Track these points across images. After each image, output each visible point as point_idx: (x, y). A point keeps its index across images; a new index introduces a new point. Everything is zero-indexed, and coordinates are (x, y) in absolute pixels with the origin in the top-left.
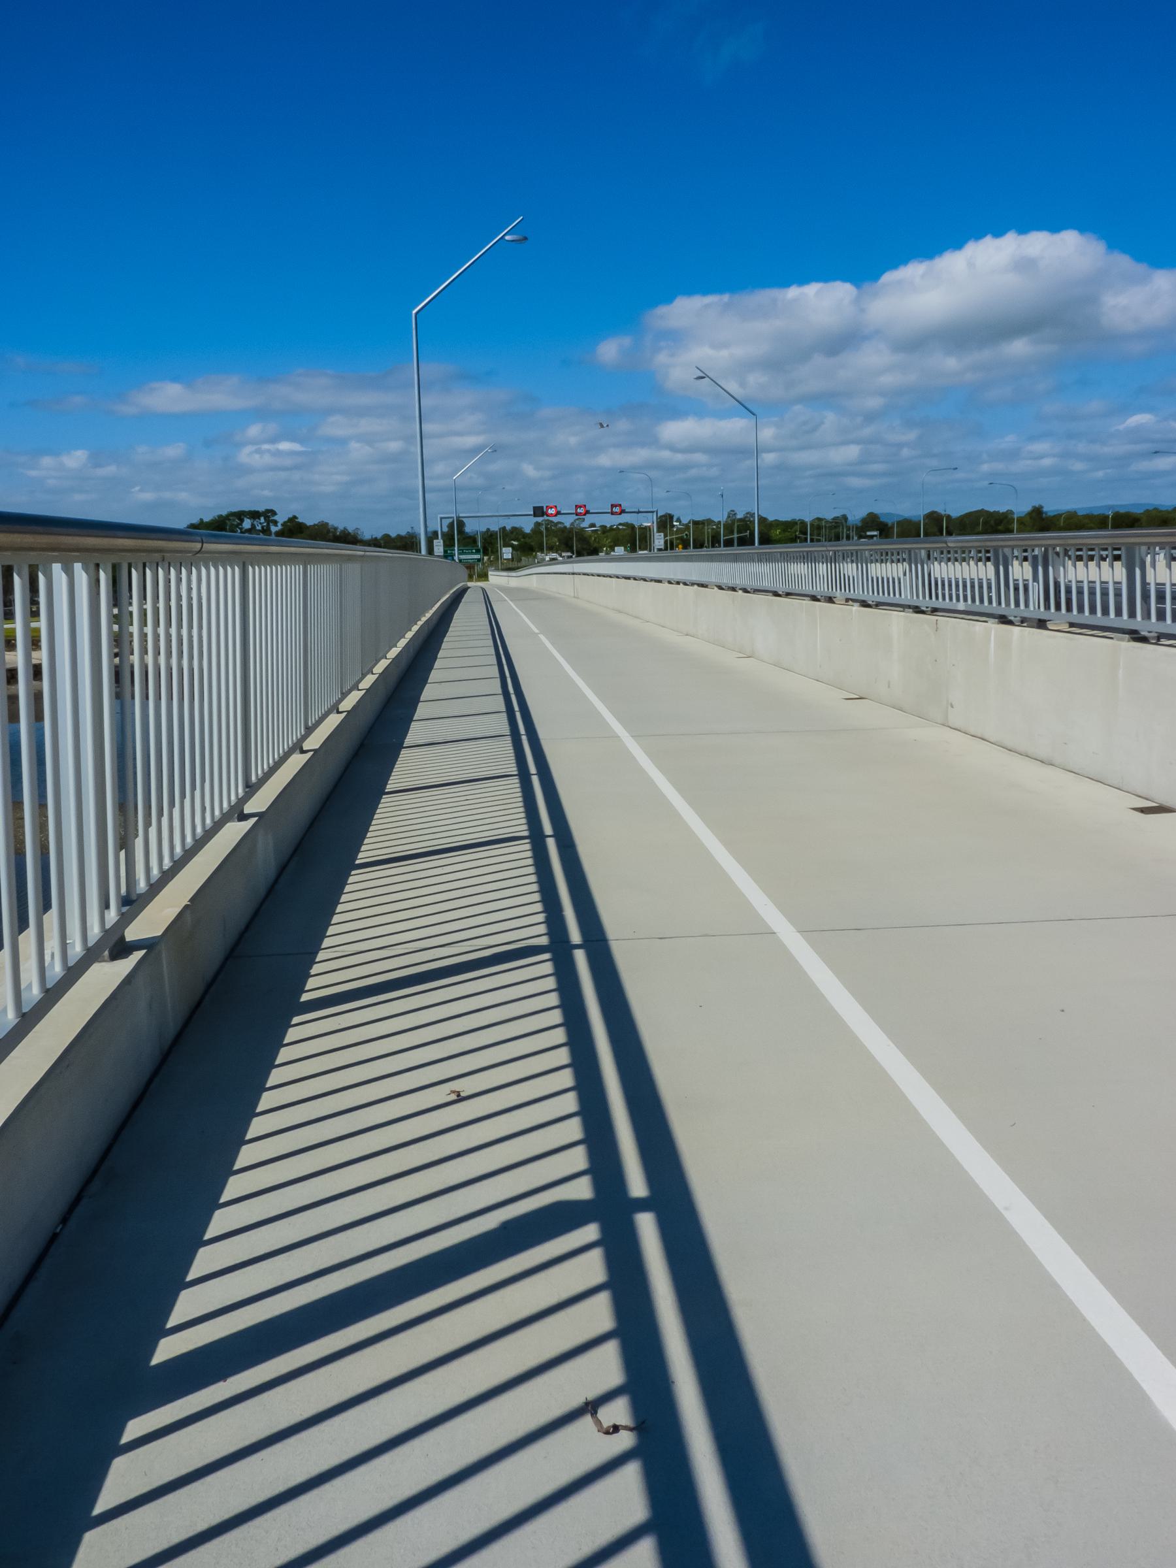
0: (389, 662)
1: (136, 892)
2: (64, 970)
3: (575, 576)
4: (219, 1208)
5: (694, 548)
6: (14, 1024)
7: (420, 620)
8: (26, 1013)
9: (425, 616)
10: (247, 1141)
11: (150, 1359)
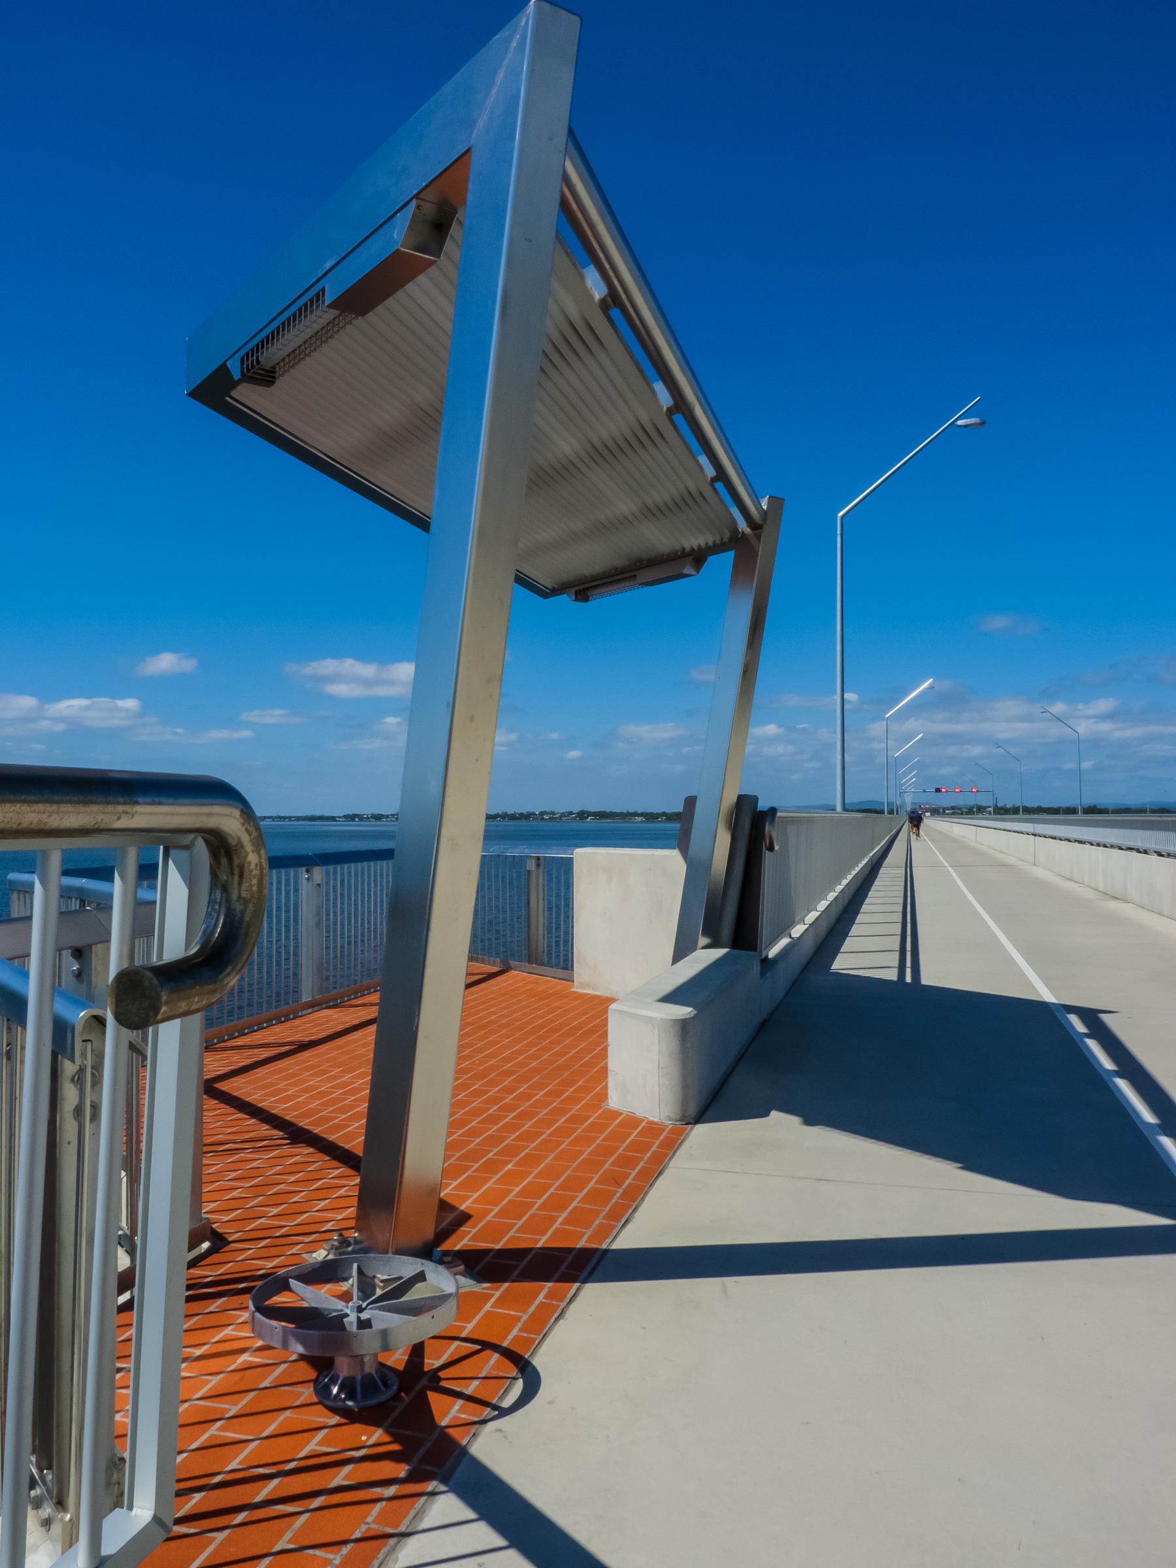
0: (818, 914)
3: (1037, 838)
5: (1023, 814)
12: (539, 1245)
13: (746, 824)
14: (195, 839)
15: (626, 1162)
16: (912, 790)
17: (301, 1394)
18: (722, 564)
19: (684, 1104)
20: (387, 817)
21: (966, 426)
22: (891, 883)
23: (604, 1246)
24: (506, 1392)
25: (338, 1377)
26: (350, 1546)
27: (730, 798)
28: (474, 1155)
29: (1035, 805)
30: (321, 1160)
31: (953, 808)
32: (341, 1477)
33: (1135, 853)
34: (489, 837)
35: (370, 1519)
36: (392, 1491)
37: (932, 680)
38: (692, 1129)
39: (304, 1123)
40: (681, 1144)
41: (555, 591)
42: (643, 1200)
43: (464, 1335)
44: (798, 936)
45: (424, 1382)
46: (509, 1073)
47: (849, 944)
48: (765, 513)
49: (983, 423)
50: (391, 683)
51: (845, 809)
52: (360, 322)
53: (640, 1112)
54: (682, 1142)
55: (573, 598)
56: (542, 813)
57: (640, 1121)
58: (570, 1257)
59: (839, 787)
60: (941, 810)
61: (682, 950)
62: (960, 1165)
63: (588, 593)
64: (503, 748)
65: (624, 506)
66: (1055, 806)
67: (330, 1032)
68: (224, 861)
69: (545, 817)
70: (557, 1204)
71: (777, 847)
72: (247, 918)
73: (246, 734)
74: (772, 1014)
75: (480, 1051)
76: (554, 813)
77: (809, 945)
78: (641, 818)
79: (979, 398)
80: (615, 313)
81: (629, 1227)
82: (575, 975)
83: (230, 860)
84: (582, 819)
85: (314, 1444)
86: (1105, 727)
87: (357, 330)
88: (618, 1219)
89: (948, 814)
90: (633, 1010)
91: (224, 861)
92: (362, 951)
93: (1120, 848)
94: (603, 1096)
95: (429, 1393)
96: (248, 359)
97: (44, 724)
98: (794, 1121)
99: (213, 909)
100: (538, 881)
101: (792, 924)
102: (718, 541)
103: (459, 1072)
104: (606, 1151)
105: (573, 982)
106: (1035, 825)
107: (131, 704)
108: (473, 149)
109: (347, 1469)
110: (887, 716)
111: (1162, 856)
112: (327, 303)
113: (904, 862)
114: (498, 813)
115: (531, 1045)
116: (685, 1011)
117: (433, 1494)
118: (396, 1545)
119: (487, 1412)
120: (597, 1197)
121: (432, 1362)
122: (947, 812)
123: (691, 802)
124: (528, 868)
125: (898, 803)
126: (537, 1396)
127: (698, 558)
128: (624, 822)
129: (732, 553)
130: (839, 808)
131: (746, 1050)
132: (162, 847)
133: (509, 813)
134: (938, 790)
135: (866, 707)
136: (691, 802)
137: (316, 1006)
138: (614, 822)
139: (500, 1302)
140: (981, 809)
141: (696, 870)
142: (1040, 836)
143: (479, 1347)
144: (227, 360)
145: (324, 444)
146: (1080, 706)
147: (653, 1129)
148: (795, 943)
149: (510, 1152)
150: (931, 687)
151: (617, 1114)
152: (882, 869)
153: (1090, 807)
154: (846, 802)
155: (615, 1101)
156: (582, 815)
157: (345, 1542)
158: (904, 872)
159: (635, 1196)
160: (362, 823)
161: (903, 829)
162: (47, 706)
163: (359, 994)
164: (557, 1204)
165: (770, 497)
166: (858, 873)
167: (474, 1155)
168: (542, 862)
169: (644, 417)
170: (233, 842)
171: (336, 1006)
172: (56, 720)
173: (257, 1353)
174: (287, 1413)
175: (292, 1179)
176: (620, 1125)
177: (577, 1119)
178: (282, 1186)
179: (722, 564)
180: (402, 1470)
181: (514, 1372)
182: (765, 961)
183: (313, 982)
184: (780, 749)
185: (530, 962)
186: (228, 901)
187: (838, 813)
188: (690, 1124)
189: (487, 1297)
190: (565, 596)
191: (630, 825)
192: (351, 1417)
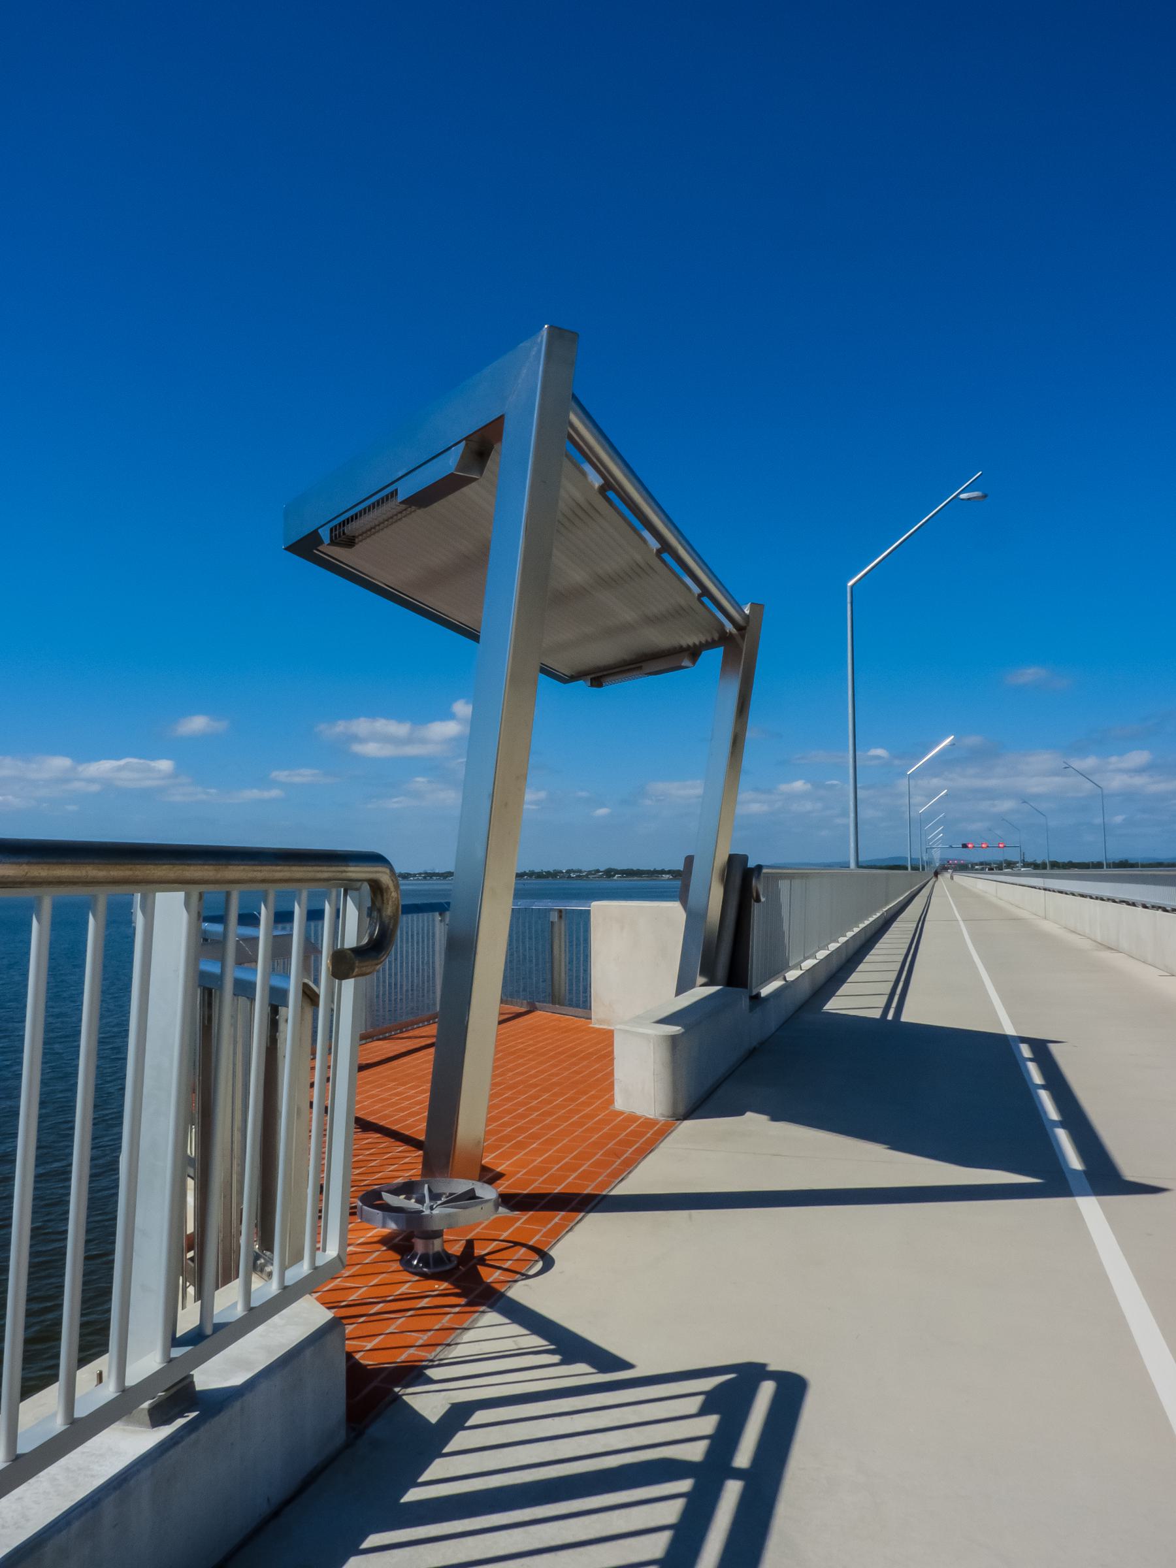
0: (816, 961)
1: (212, 1321)
2: (244, 1311)
3: (1047, 892)
4: (440, 1457)
5: (1107, 868)
6: (275, 1294)
7: (871, 917)
8: (255, 1307)
9: (876, 915)
10: (444, 1454)
11: (360, 1545)
12: (556, 1191)
13: (737, 881)
14: (361, 885)
15: (627, 1143)
16: (940, 846)
17: (391, 1266)
18: (713, 657)
19: (675, 1104)
20: (414, 875)
21: (969, 499)
22: (899, 936)
23: (604, 1193)
24: (530, 1268)
25: (417, 1254)
26: (432, 1332)
27: (722, 859)
28: (507, 1138)
29: (1066, 860)
30: (387, 1142)
31: (981, 864)
32: (424, 1303)
33: (1125, 906)
34: (518, 894)
35: (444, 1321)
36: (457, 1309)
37: (952, 737)
38: (680, 1124)
39: (371, 1119)
40: (670, 1134)
41: (573, 678)
42: (636, 1167)
43: (501, 1238)
44: (792, 979)
45: (475, 1261)
46: (535, 1085)
47: (845, 989)
48: (748, 616)
49: (985, 496)
50: (423, 741)
51: (858, 866)
52: (420, 512)
53: (639, 1112)
54: (672, 1132)
55: (589, 684)
56: (569, 872)
57: (637, 1118)
58: (578, 1199)
59: (852, 845)
60: (970, 866)
61: (683, 986)
62: (888, 1146)
63: (602, 680)
64: (534, 807)
65: (628, 615)
66: (1086, 861)
67: (383, 1057)
68: (379, 897)
69: (572, 875)
70: (570, 1168)
71: (763, 899)
72: (391, 927)
73: (275, 793)
74: (762, 1044)
75: (511, 1070)
76: (580, 871)
77: (806, 989)
78: (668, 876)
79: (980, 473)
80: (611, 494)
81: (623, 1183)
82: (593, 1013)
83: (382, 896)
84: (609, 877)
85: (404, 1289)
86: (1139, 781)
87: (420, 515)
88: (616, 1178)
89: (977, 870)
90: (634, 1029)
91: (379, 897)
92: (401, 999)
93: (1114, 901)
94: (611, 1101)
95: (478, 1267)
96: (336, 530)
97: (77, 785)
98: (763, 1119)
99: (373, 921)
100: (561, 929)
101: (787, 967)
102: (709, 640)
103: (494, 1085)
104: (610, 1136)
105: (591, 1019)
106: (1045, 880)
107: (165, 765)
108: (506, 416)
109: (427, 1300)
110: (908, 773)
111: (1167, 911)
112: (399, 501)
113: (919, 916)
114: (525, 872)
115: (555, 1066)
116: (675, 1029)
117: (483, 1312)
118: (461, 1333)
119: (518, 1276)
120: (601, 1164)
121: (479, 1251)
122: (976, 867)
123: (689, 860)
124: (551, 920)
125: (925, 858)
126: (549, 1272)
127: (694, 653)
128: (651, 880)
129: (722, 649)
130: (853, 865)
131: (734, 1071)
132: (342, 890)
133: (536, 871)
134: (965, 846)
135: (897, 762)
136: (689, 860)
137: (368, 1038)
138: (640, 880)
139: (527, 1222)
140: (1010, 865)
141: (694, 918)
142: (1049, 890)
143: (512, 1244)
144: (319, 528)
145: (382, 577)
146: (1114, 759)
147: (649, 1123)
148: (788, 986)
149: (535, 1137)
150: (952, 744)
151: (622, 1113)
152: (895, 923)
153: (1121, 861)
154: (860, 859)
155: (620, 1104)
156: (609, 873)
157: (430, 1330)
158: (915, 925)
159: (630, 1164)
160: (426, 882)
161: (927, 886)
162: (80, 768)
163: (404, 1030)
164: (570, 1168)
165: (752, 603)
166: (871, 923)
167: (507, 1138)
168: (563, 914)
169: (638, 558)
170: (384, 887)
171: (385, 1039)
172: (91, 780)
173: (359, 1246)
174: (384, 1275)
175: (368, 1153)
176: (623, 1120)
177: (589, 1117)
178: (360, 1157)
179: (713, 657)
180: (463, 1301)
181: (537, 1257)
182: (756, 998)
183: (366, 1015)
184: (809, 806)
185: (553, 1003)
186: (381, 917)
187: (852, 870)
188: (681, 1120)
189: (518, 1219)
190: (581, 682)
191: (656, 883)
192: (426, 1277)
